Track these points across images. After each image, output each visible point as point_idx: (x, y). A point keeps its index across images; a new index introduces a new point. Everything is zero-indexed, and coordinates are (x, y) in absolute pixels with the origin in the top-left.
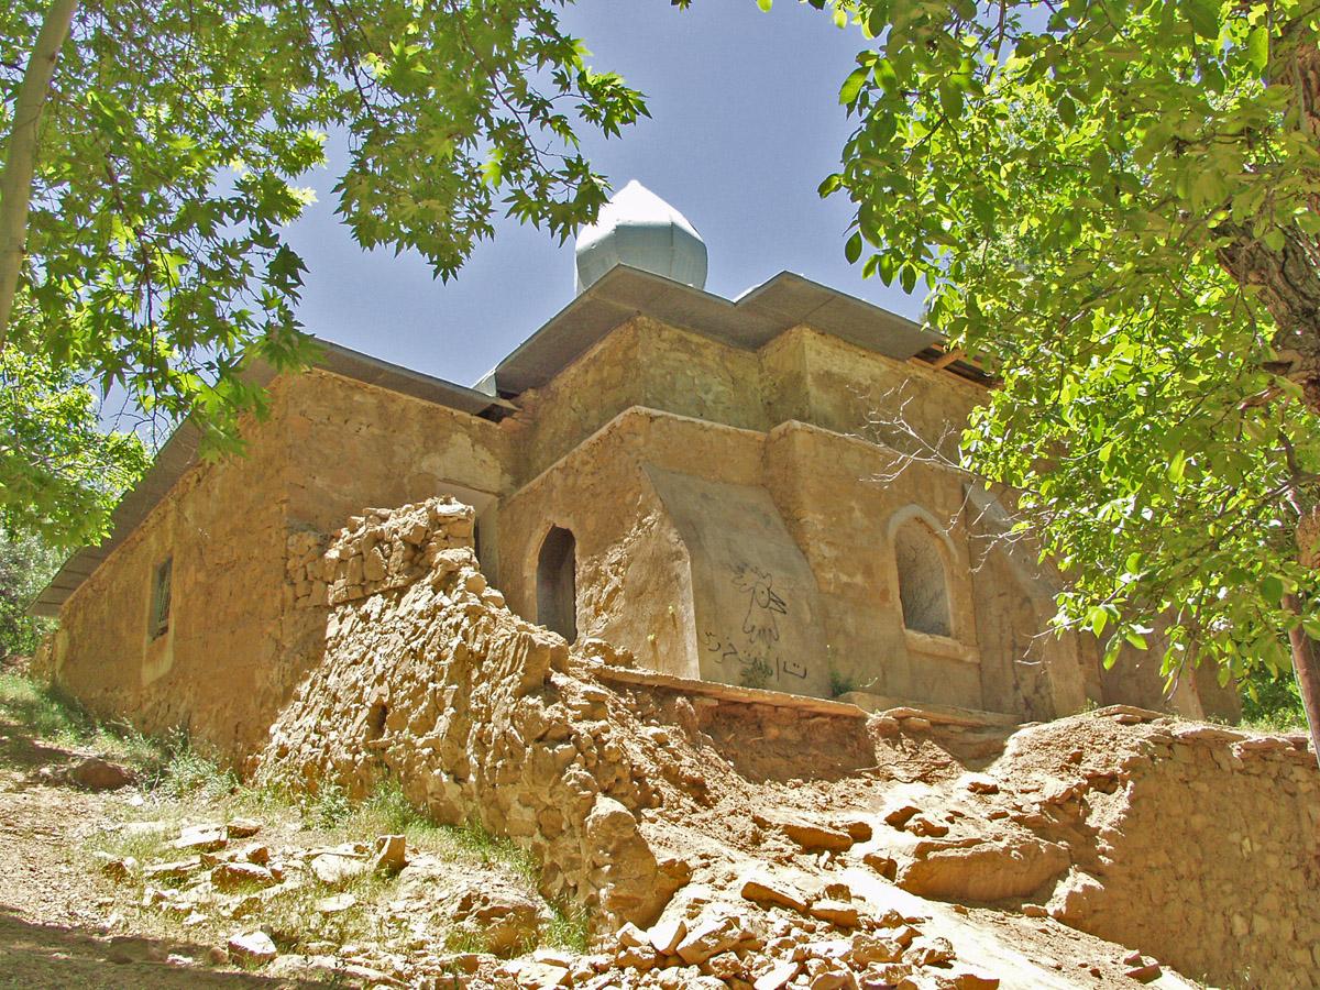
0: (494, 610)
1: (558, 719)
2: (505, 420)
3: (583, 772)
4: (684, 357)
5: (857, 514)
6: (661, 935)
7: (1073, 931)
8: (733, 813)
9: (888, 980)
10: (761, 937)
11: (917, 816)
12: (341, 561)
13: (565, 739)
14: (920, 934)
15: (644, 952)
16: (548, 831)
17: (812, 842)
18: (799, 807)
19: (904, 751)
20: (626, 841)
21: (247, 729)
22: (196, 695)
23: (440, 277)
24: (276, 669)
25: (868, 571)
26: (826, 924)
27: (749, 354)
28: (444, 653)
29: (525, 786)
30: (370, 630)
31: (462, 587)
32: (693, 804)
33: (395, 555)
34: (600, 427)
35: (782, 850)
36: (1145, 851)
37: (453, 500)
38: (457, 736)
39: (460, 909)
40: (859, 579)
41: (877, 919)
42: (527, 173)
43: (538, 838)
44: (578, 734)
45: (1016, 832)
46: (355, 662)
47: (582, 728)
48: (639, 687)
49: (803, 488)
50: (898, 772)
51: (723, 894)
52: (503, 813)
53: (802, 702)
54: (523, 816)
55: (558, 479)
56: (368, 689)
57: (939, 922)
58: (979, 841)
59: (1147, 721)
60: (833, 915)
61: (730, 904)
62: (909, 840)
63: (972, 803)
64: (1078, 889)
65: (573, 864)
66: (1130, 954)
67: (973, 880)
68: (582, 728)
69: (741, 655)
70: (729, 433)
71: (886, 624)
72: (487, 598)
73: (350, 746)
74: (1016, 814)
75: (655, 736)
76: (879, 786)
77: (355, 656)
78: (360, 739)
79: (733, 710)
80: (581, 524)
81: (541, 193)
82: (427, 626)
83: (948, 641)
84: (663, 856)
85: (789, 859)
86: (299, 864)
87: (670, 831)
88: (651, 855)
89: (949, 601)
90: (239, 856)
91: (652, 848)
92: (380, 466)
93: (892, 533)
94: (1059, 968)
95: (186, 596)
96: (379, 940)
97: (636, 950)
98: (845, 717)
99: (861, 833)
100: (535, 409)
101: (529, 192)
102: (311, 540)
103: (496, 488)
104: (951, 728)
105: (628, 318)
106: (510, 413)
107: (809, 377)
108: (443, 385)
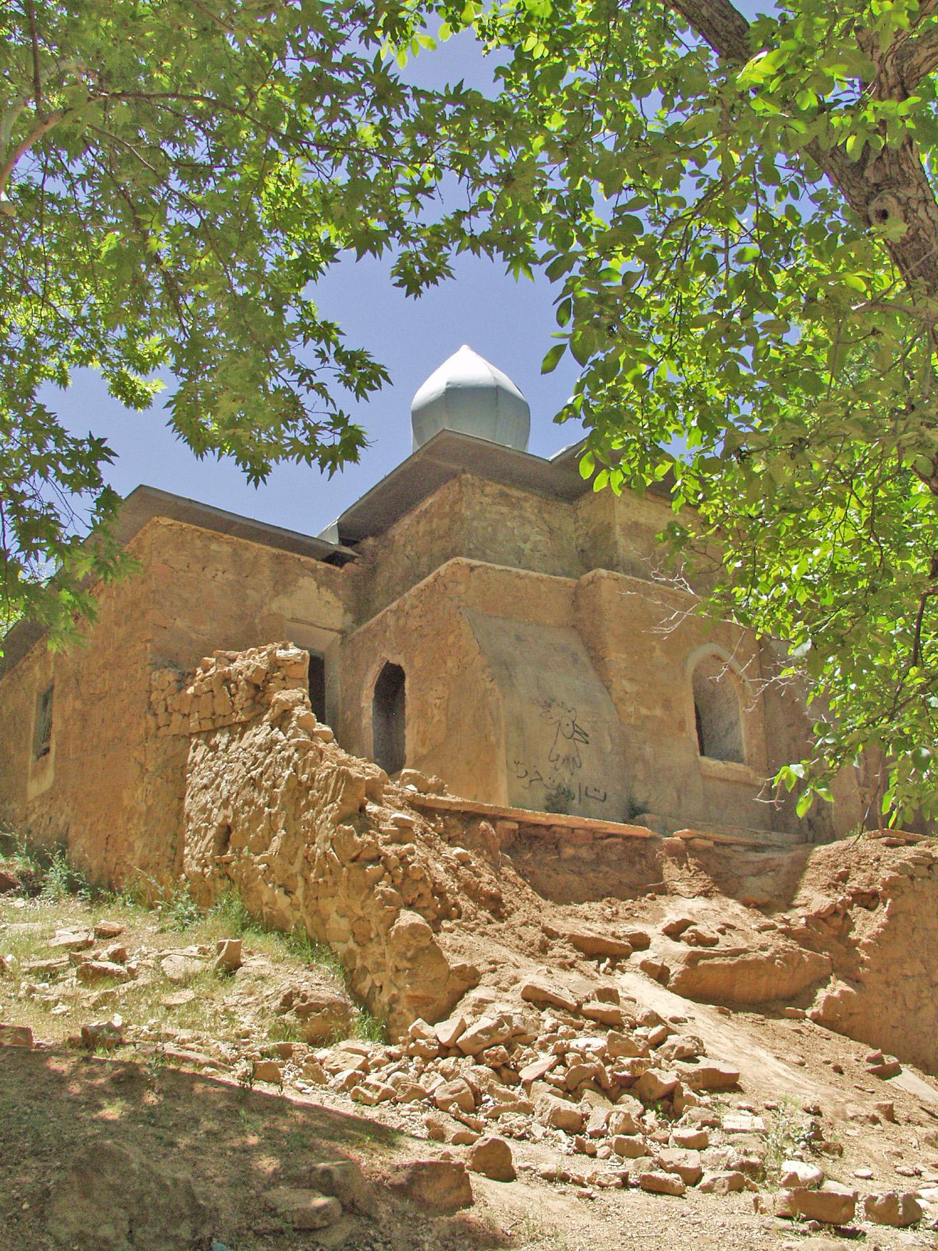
0: (321, 745)
1: (369, 843)
2: (347, 565)
3: (390, 889)
4: (505, 510)
5: (658, 653)
6: (444, 1031)
7: (826, 1031)
8: (525, 924)
9: (633, 1073)
10: (531, 1033)
11: (692, 928)
12: (195, 696)
13: (375, 860)
14: (674, 1033)
15: (430, 1044)
16: (360, 939)
17: (594, 950)
18: (587, 919)
19: (688, 868)
20: (423, 949)
21: (115, 841)
22: (73, 809)
23: (252, 482)
24: (140, 790)
25: (667, 705)
26: (593, 1023)
27: (565, 505)
28: (278, 782)
29: (341, 900)
30: (219, 759)
31: (294, 724)
32: (489, 916)
33: (241, 693)
34: (429, 573)
35: (566, 957)
36: (901, 962)
37: (291, 645)
38: (287, 855)
39: (282, 1004)
40: (658, 712)
41: (638, 1019)
42: (300, 424)
43: (351, 944)
44: (386, 856)
45: (781, 943)
46: (206, 787)
47: (390, 850)
48: (447, 812)
49: (608, 629)
50: (681, 887)
51: (508, 996)
52: (324, 922)
53: (595, 825)
54: (339, 925)
55: (391, 620)
56: (215, 811)
57: (703, 1023)
58: (745, 951)
59: (910, 843)
60: (599, 1015)
61: (510, 1006)
62: (682, 948)
63: (745, 916)
64: (836, 994)
65: (379, 967)
66: (872, 1052)
67: (736, 990)
68: (390, 850)
69: (546, 780)
70: (542, 581)
71: (682, 750)
72: (317, 734)
73: (200, 860)
74: (783, 926)
75: (458, 856)
76: (661, 900)
77: (205, 781)
78: (208, 854)
79: (533, 832)
80: (410, 660)
81: (312, 440)
82: (265, 758)
83: (740, 767)
84: (456, 961)
85: (572, 965)
86: (150, 962)
87: (466, 940)
88: (444, 961)
89: (743, 731)
90: (102, 957)
91: (446, 954)
92: (234, 609)
93: (690, 670)
94: (802, 1064)
95: (66, 721)
96: (211, 1029)
97: (422, 1042)
98: (637, 838)
99: (641, 942)
100: (374, 554)
101: (302, 439)
102: (170, 676)
103: (339, 626)
104: (734, 848)
105: (454, 475)
106: (351, 559)
107: (618, 529)
108: (290, 535)
